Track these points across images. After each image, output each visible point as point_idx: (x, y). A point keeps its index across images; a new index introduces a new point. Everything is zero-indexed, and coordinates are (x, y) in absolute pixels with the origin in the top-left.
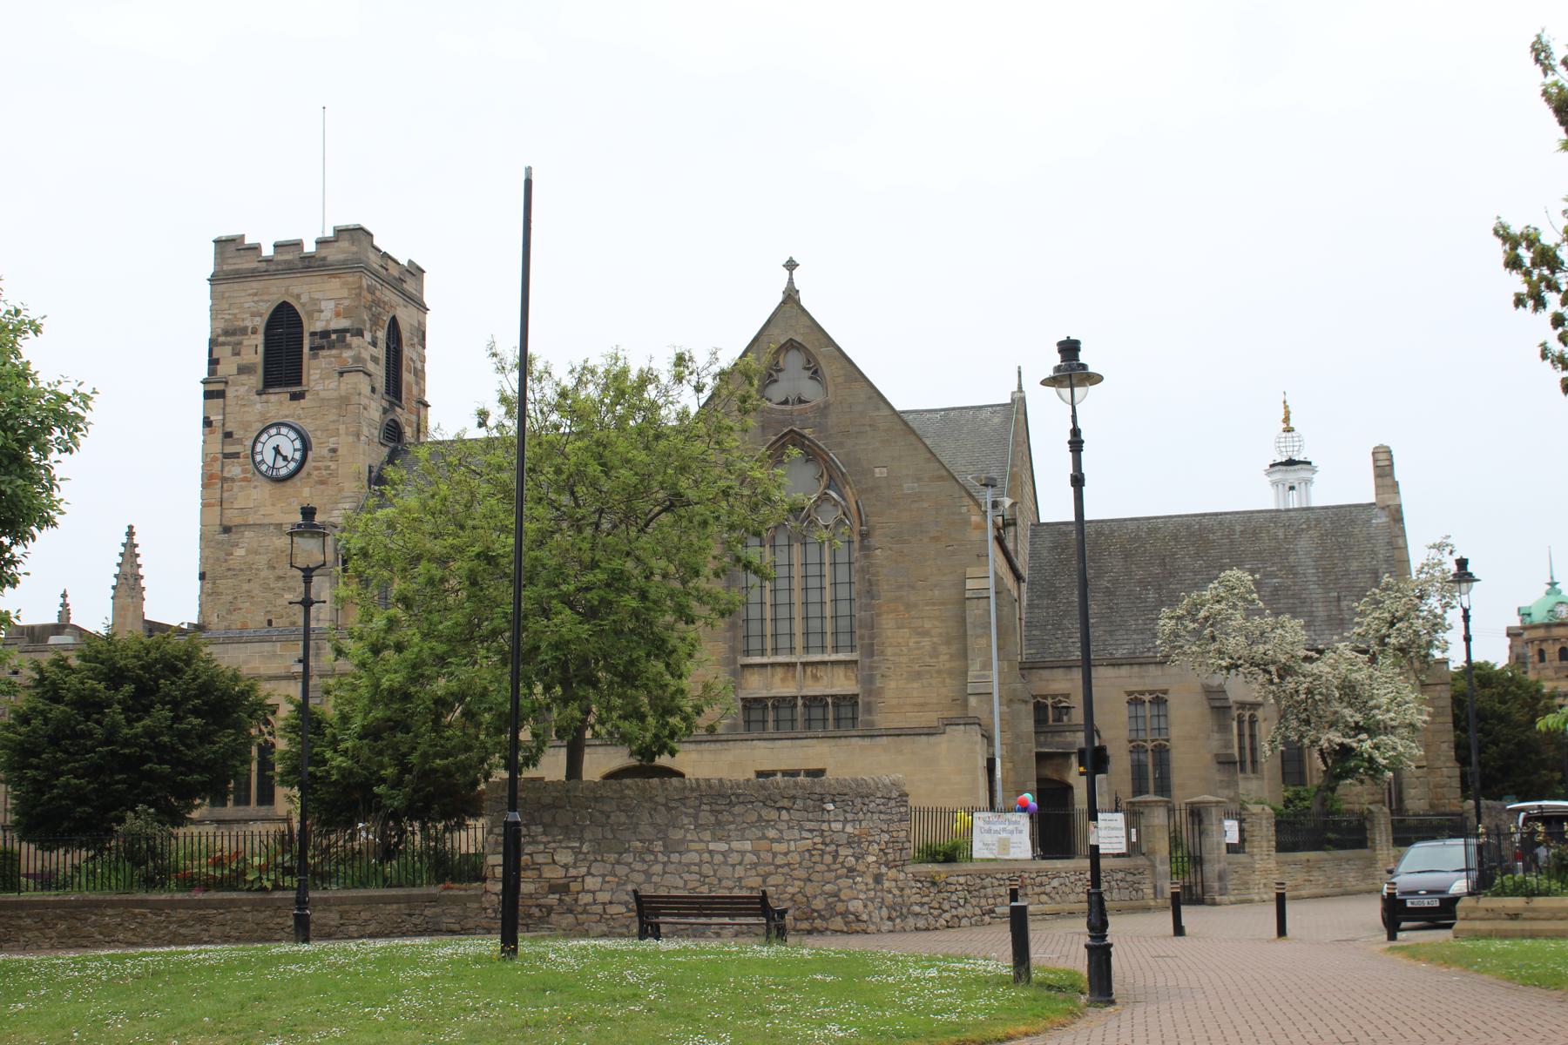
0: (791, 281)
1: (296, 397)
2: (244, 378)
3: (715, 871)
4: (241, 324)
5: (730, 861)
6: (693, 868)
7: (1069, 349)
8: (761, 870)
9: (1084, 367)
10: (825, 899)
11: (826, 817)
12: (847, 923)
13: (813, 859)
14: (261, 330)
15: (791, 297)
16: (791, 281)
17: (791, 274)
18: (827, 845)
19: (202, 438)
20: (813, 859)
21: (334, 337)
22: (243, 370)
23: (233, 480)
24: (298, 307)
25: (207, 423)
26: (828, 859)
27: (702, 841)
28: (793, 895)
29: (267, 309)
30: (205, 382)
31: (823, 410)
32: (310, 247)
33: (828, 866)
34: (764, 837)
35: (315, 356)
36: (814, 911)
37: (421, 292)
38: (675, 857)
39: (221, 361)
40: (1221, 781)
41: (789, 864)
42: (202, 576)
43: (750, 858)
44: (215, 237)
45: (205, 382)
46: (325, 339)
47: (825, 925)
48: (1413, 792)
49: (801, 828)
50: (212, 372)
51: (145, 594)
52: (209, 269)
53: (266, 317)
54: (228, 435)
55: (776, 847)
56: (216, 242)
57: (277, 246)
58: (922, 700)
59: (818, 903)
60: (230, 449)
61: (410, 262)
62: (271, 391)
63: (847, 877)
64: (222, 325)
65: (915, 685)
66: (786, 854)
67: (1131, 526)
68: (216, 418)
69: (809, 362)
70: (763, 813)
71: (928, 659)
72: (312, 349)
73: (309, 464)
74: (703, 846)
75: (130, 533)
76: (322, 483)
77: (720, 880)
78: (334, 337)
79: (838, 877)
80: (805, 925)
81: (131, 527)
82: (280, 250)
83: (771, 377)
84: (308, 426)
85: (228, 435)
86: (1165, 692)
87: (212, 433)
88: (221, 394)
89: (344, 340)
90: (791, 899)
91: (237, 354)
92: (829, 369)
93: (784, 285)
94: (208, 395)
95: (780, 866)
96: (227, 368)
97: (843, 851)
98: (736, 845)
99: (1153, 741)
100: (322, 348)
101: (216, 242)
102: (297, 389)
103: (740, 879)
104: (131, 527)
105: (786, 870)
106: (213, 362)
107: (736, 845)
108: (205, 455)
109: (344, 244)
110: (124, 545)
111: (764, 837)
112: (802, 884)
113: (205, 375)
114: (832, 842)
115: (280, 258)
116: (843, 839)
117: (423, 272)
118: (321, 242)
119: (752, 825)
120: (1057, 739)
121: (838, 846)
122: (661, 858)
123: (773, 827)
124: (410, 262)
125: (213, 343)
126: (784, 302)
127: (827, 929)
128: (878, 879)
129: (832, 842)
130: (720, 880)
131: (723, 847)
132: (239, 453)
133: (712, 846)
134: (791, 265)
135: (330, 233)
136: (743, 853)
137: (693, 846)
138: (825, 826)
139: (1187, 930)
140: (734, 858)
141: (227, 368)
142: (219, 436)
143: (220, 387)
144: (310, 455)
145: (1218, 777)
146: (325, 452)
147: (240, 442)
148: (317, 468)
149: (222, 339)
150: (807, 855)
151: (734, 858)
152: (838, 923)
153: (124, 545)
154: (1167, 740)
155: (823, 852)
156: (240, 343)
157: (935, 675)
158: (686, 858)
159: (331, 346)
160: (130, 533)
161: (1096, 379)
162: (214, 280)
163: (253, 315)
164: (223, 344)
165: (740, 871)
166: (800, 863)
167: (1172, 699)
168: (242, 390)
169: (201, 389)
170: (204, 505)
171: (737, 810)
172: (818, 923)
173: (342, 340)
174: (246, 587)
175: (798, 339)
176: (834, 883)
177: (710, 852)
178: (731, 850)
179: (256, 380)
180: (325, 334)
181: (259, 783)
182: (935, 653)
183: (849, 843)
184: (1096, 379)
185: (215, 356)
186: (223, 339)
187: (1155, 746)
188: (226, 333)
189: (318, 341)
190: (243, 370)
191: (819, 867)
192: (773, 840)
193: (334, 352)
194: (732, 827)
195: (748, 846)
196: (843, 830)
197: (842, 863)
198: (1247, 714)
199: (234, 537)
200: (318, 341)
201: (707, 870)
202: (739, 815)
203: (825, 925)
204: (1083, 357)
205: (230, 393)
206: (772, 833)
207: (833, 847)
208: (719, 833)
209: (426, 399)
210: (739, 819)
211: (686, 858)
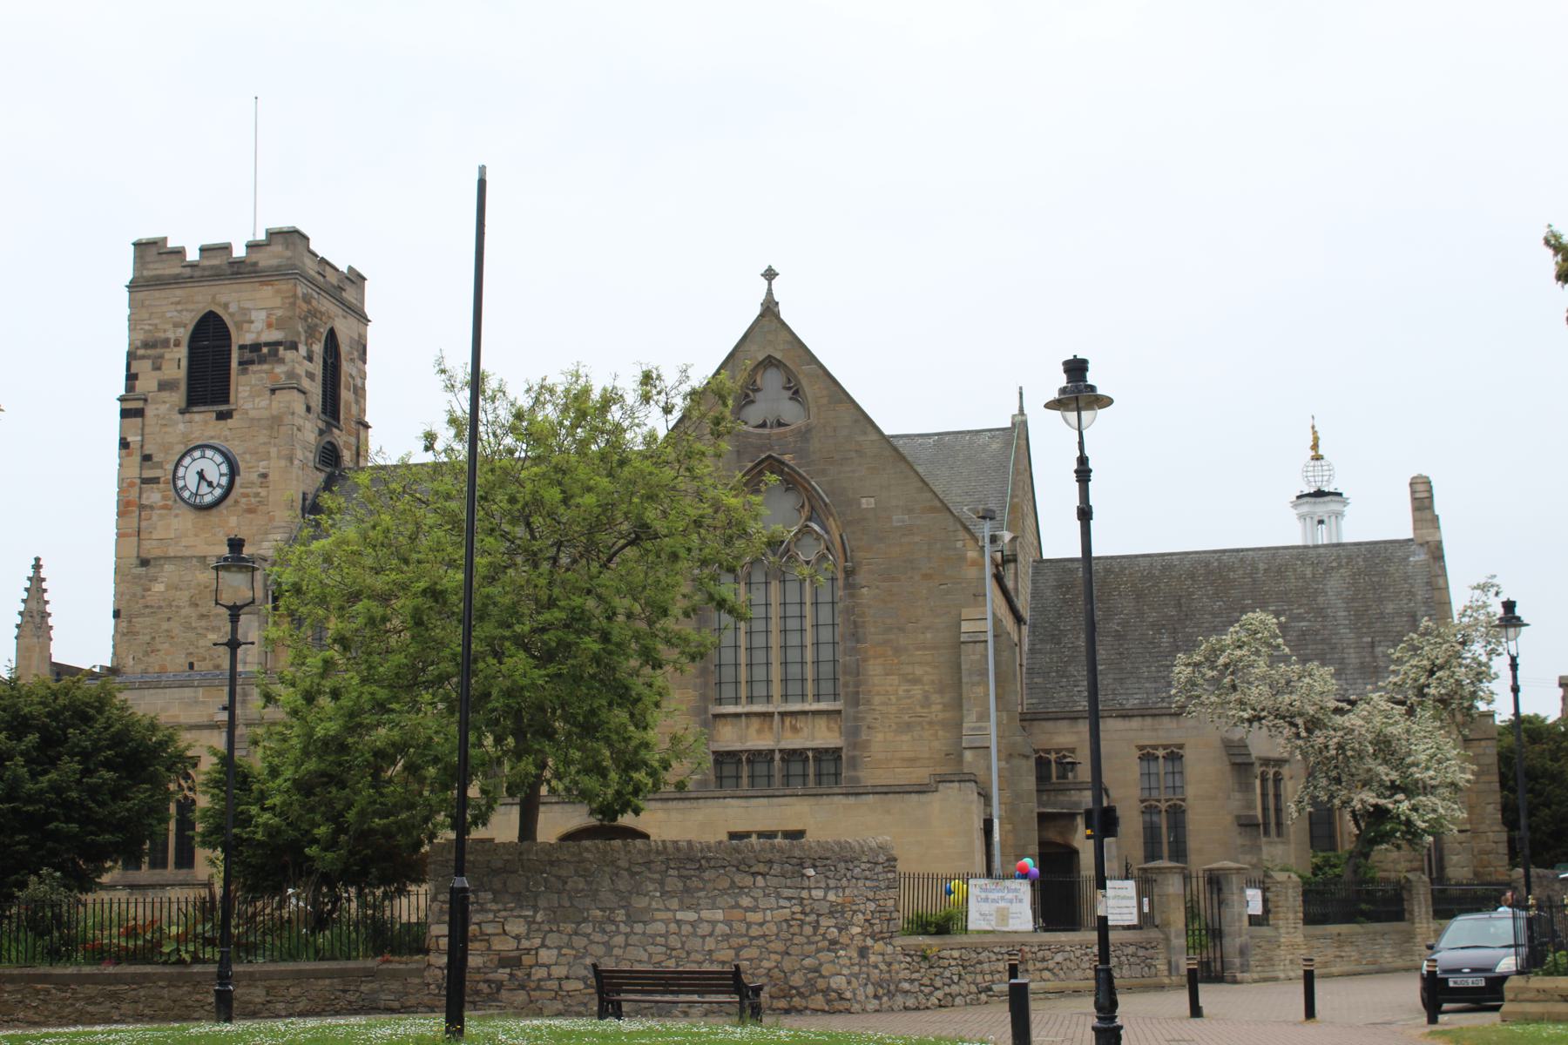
0: (770, 292)
1: (222, 416)
2: (165, 395)
3: (683, 944)
4: (162, 335)
5: (700, 932)
7: (1076, 368)
9: (1092, 388)
10: (805, 974)
12: (828, 1002)
15: (770, 309)
16: (770, 292)
17: (770, 284)
19: (118, 461)
21: (265, 350)
22: (164, 386)
24: (226, 318)
25: (124, 444)
26: (808, 930)
27: (669, 910)
28: (770, 970)
29: (191, 319)
30: (122, 399)
31: (805, 434)
32: (239, 252)
33: (808, 937)
34: (737, 906)
35: (244, 372)
37: (362, 302)
38: (639, 928)
39: (140, 377)
40: (1243, 846)
41: (764, 936)
42: (117, 614)
43: (721, 928)
45: (122, 399)
46: (256, 353)
48: (1455, 858)
49: (779, 896)
50: (130, 387)
52: (128, 274)
53: (191, 327)
54: (147, 458)
55: (751, 916)
56: (134, 244)
57: (203, 250)
58: (911, 755)
59: (797, 980)
60: (148, 474)
61: (351, 269)
62: (195, 409)
63: (829, 950)
64: (141, 336)
65: (906, 737)
66: (761, 925)
67: (1144, 563)
69: (789, 381)
71: (918, 709)
72: (240, 363)
75: (37, 566)
76: (251, 511)
77: (688, 953)
78: (265, 350)
79: (818, 951)
80: (782, 1004)
81: (38, 560)
82: (207, 254)
83: (747, 397)
84: (236, 448)
85: (147, 458)
86: (1181, 746)
87: (129, 455)
88: (139, 413)
89: (276, 354)
91: (157, 368)
92: (810, 389)
93: (762, 296)
94: (125, 414)
96: (147, 384)
97: (824, 922)
98: (706, 914)
99: (1167, 801)
100: (252, 362)
101: (134, 244)
102: (223, 408)
103: (710, 952)
104: (38, 560)
105: (761, 942)
106: (131, 377)
107: (706, 914)
109: (277, 248)
110: (30, 579)
111: (737, 906)
112: (778, 957)
114: (812, 911)
115: (206, 263)
117: (364, 279)
118: (252, 246)
119: (724, 892)
120: (1061, 798)
121: (819, 915)
123: (747, 895)
124: (351, 269)
125: (131, 356)
126: (762, 315)
127: (806, 1008)
129: (812, 911)
130: (688, 953)
132: (159, 478)
133: (679, 915)
134: (770, 275)
135: (261, 236)
136: (713, 923)
137: (659, 915)
138: (805, 894)
139: (1205, 1011)
140: (704, 929)
141: (147, 384)
142: (137, 458)
143: (138, 405)
144: (238, 480)
146: (254, 477)
148: (245, 495)
149: (141, 352)
150: (785, 926)
151: (704, 929)
153: (30, 579)
154: (1183, 800)
156: (161, 357)
157: (927, 727)
158: (651, 929)
159: (262, 360)
160: (37, 566)
161: (1105, 402)
162: (133, 287)
163: (176, 325)
164: (143, 357)
165: (710, 944)
166: (777, 935)
167: (1189, 754)
168: (163, 408)
169: (117, 407)
170: (120, 535)
171: (706, 875)
172: (797, 1001)
174: (165, 626)
175: (778, 356)
176: (815, 957)
177: (678, 922)
178: (700, 920)
179: (178, 397)
180: (256, 347)
182: (926, 702)
183: (831, 912)
184: (1105, 402)
185: (133, 371)
187: (1170, 806)
188: (146, 345)
189: (247, 355)
190: (164, 386)
192: (747, 909)
193: (265, 367)
194: (702, 894)
195: (719, 915)
196: (824, 899)
199: (152, 571)
200: (247, 355)
201: (674, 941)
204: (1091, 378)
205: (150, 411)
206: (746, 901)
207: (813, 917)
209: (367, 419)
210: (710, 885)
211: (651, 929)
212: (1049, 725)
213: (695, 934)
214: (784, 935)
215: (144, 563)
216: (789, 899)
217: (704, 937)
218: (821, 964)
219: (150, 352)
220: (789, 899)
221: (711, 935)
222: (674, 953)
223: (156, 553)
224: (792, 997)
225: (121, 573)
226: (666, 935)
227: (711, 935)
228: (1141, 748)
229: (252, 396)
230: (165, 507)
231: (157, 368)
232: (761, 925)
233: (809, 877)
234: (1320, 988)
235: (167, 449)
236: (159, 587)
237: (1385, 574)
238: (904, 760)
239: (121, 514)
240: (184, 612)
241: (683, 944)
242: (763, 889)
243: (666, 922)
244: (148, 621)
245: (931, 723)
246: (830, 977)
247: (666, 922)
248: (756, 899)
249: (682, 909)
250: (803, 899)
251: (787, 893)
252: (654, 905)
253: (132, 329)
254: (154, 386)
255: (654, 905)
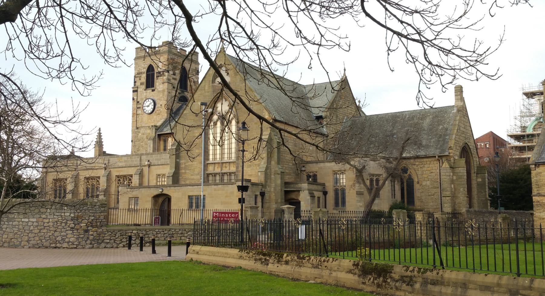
1: (153, 91)
2: (141, 86)
3: (24, 228)
4: (141, 71)
5: (29, 225)
6: (17, 227)
8: (39, 227)
10: (62, 237)
11: (63, 211)
12: (69, 245)
13: (58, 225)
14: (145, 73)
18: (63, 220)
20: (58, 225)
22: (142, 84)
23: (139, 114)
25: (133, 99)
26: (63, 224)
27: (19, 218)
28: (50, 236)
29: (147, 66)
33: (63, 227)
34: (40, 217)
35: (157, 79)
36: (57, 241)
37: (197, 59)
38: (11, 223)
40: (357, 200)
41: (49, 226)
42: (132, 141)
43: (35, 224)
44: (136, 47)
45: (133, 88)
47: (61, 245)
48: (446, 205)
49: (54, 215)
50: (135, 85)
51: (103, 146)
52: (134, 56)
53: (147, 68)
54: (138, 102)
55: (45, 220)
58: (251, 174)
59: (59, 239)
60: (138, 106)
63: (70, 230)
64: (137, 72)
65: (249, 169)
66: (48, 223)
67: (375, 117)
68: (135, 98)
70: (41, 210)
72: (157, 77)
73: (156, 109)
74: (19, 220)
75: (100, 130)
76: (159, 114)
77: (25, 230)
79: (67, 230)
80: (54, 245)
81: (100, 128)
84: (156, 99)
85: (138, 102)
86: (316, 172)
87: (134, 102)
90: (49, 237)
91: (140, 79)
94: (134, 91)
95: (46, 227)
96: (138, 84)
97: (69, 222)
98: (31, 220)
100: (159, 76)
102: (153, 88)
103: (32, 230)
104: (100, 128)
105: (48, 228)
106: (135, 82)
107: (31, 220)
108: (133, 108)
111: (40, 217)
112: (53, 232)
113: (133, 86)
114: (65, 219)
116: (70, 218)
119: (36, 214)
120: (297, 186)
121: (67, 220)
122: (6, 223)
123: (44, 214)
125: (135, 77)
127: (61, 247)
128: (86, 231)
129: (65, 219)
130: (25, 230)
131: (27, 220)
133: (23, 220)
136: (33, 222)
137: (17, 220)
138: (63, 214)
139: (157, 252)
140: (30, 224)
141: (138, 84)
142: (136, 102)
143: (136, 89)
144: (156, 107)
145: (357, 199)
146: (159, 106)
147: (141, 104)
148: (158, 110)
149: (137, 76)
150: (56, 223)
151: (30, 224)
152: (65, 245)
155: (62, 223)
156: (141, 77)
158: (14, 223)
160: (100, 130)
162: (135, 59)
163: (144, 68)
164: (137, 77)
165: (32, 228)
166: (53, 226)
167: (159, 173)
168: (141, 89)
169: (132, 90)
170: (133, 122)
171: (31, 209)
172: (58, 245)
173: (163, 74)
174: (141, 144)
176: (65, 232)
177: (23, 222)
178: (29, 221)
179: (144, 87)
180: (159, 73)
181: (407, 190)
183: (71, 220)
186: (137, 76)
188: (138, 74)
189: (158, 75)
190: (142, 84)
191: (60, 227)
192: (44, 218)
193: (162, 77)
194: (30, 214)
195: (35, 220)
196: (70, 216)
197: (69, 226)
198: (375, 178)
199: (139, 130)
201: (21, 227)
202: (32, 210)
203: (61, 245)
205: (139, 90)
206: (44, 216)
207: (65, 221)
208: (26, 215)
210: (33, 212)
211: (14, 223)
212: (310, 165)
213: (27, 225)
214: (55, 226)
215: (137, 128)
216: (58, 216)
217: (30, 226)
218: (67, 234)
219: (139, 75)
220: (58, 216)
221: (32, 225)
222: (21, 230)
223: (140, 126)
224: (57, 244)
225: (133, 132)
226: (19, 225)
227: (32, 225)
228: (334, 171)
229: (159, 85)
230: (142, 114)
231: (140, 79)
232: (48, 223)
233: (65, 209)
234: (173, 248)
235: (142, 99)
236: (140, 134)
237: (443, 117)
238: (249, 175)
239: (133, 116)
240: (145, 140)
241: (24, 228)
242: (50, 213)
243: (19, 222)
244: (138, 142)
245: (256, 165)
246: (70, 238)
247: (19, 222)
248: (47, 216)
249: (24, 218)
250: (62, 216)
251: (57, 214)
252: (16, 217)
253: (135, 70)
254: (139, 84)
255: (16, 217)
